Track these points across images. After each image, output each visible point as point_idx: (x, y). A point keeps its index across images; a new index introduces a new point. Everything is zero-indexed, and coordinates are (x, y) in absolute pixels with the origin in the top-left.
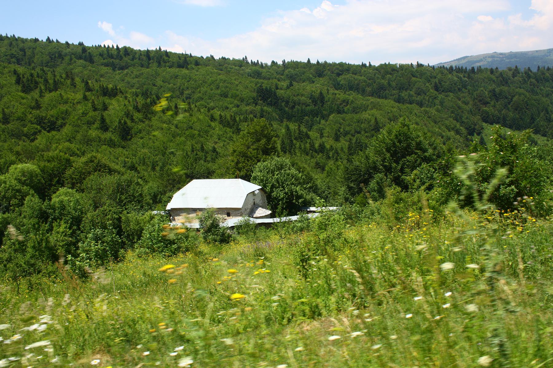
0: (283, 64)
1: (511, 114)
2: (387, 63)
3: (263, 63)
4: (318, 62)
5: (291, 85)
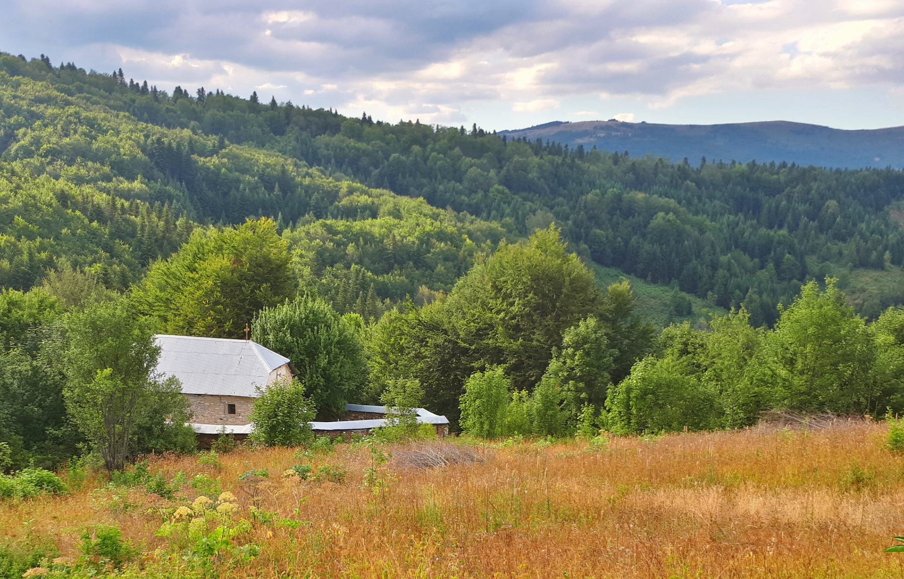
0: (199, 99)
1: (647, 247)
2: (414, 122)
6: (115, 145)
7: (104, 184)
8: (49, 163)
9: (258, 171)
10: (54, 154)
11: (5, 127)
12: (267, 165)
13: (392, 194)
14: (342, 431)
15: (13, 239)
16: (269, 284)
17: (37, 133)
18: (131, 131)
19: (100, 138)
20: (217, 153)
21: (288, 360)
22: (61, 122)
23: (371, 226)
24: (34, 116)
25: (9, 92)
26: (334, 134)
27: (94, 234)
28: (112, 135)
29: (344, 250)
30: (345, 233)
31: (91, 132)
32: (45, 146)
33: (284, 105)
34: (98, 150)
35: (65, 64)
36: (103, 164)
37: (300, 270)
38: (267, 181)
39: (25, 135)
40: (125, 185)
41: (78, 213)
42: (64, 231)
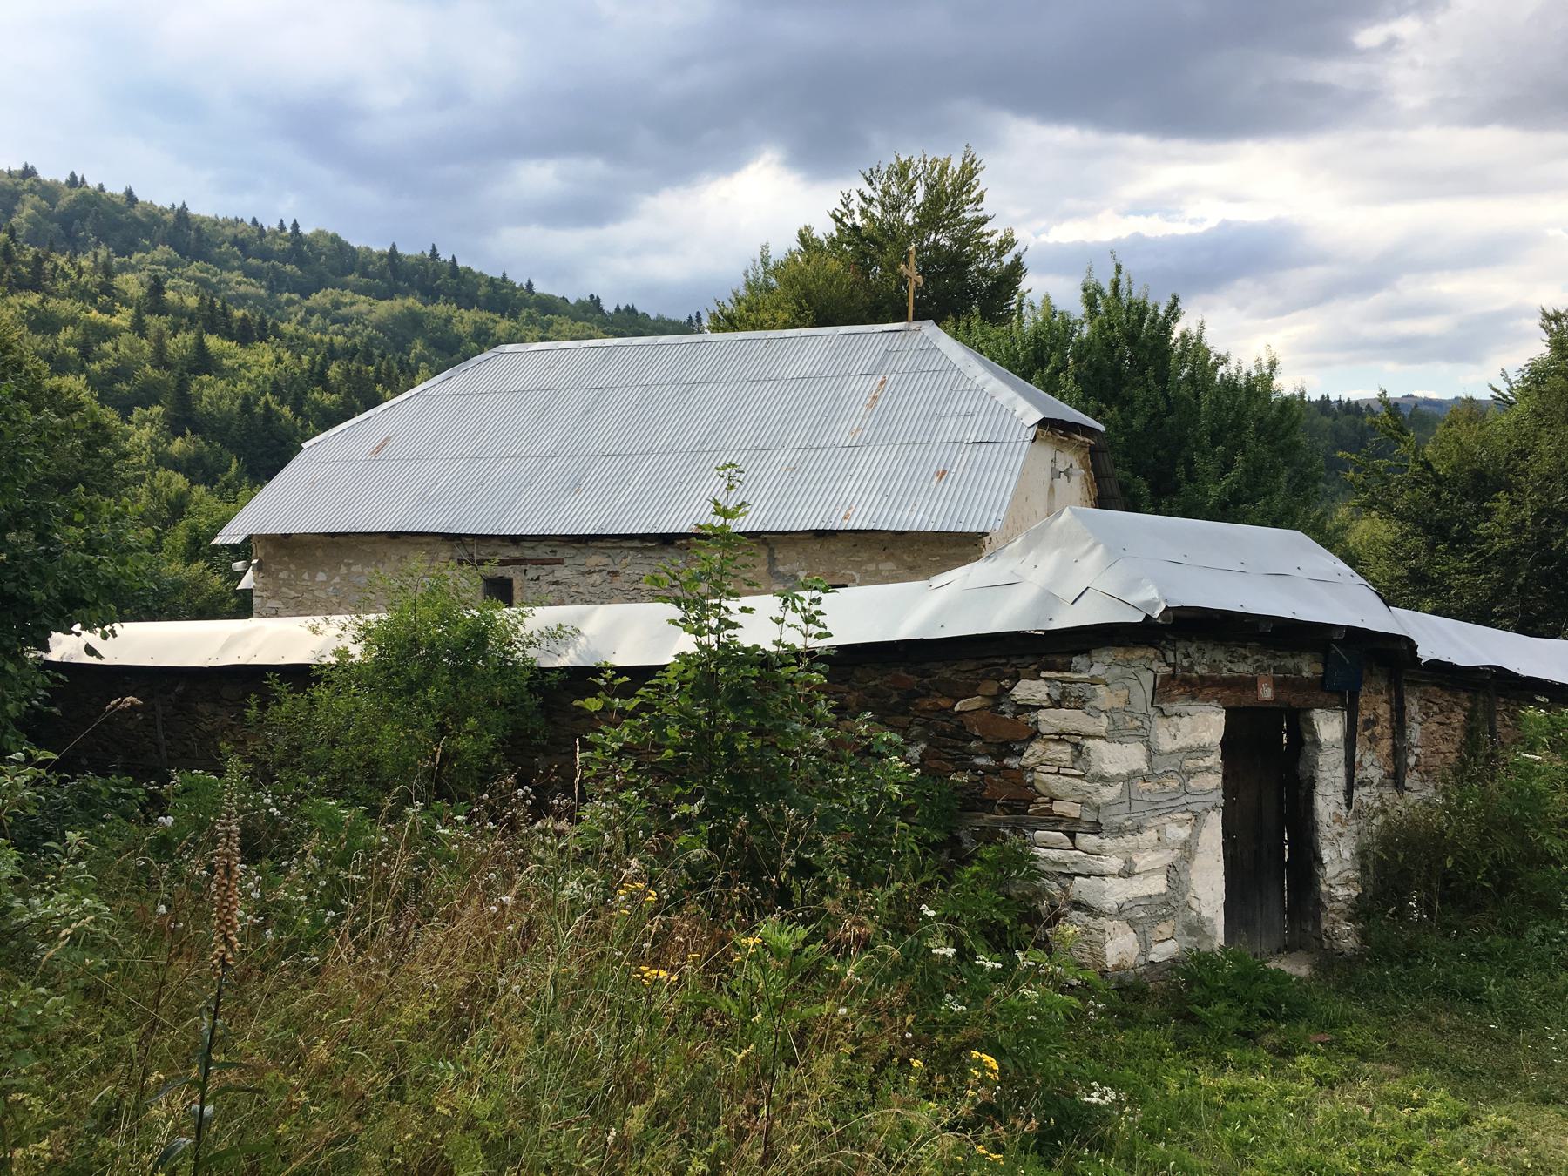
35: (622, 307)
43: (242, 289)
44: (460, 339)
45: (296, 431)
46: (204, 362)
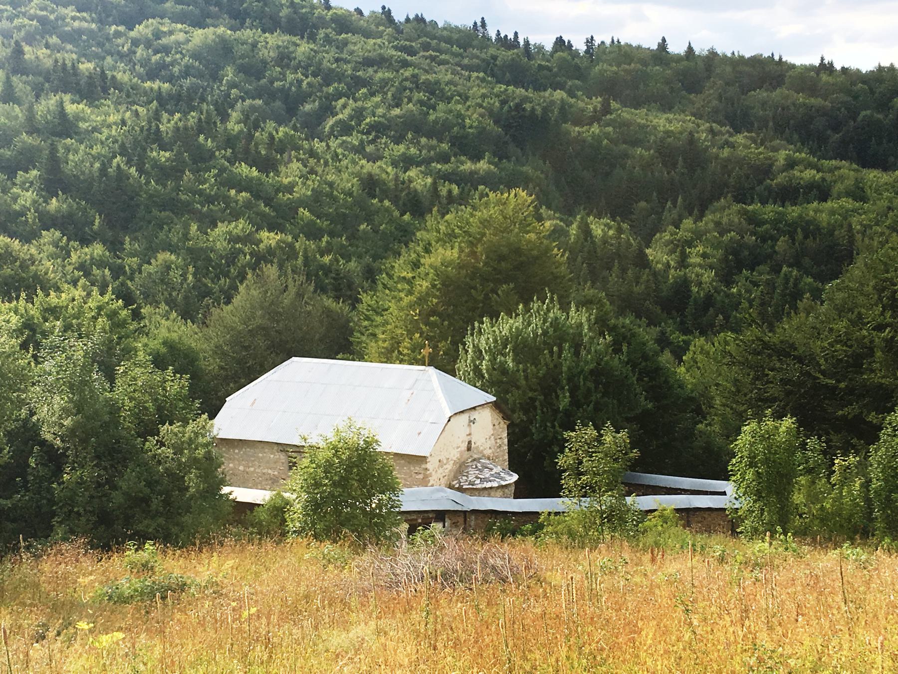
0: (587, 52)
3: (532, 42)
4: (690, 49)
5: (606, 110)
6: (459, 115)
7: (439, 166)
8: (373, 142)
9: (655, 142)
10: (379, 129)
11: (320, 98)
12: (668, 133)
13: (855, 166)
14: (505, 513)
15: (290, 239)
16: (512, 285)
17: (360, 103)
18: (484, 96)
19: (441, 106)
20: (599, 120)
21: (494, 399)
22: (393, 89)
23: (816, 211)
24: (359, 82)
25: (332, 54)
26: (775, 88)
27: (406, 231)
28: (458, 102)
29: (773, 247)
30: (775, 223)
31: (429, 99)
32: (368, 120)
33: (705, 53)
34: (436, 122)
35: (411, 17)
36: (441, 141)
37: (697, 275)
38: (667, 152)
39: (344, 106)
40: (468, 166)
41: (387, 203)
42: (363, 227)
43: (76, 24)
44: (264, 63)
45: (141, 186)
46: (64, 126)
